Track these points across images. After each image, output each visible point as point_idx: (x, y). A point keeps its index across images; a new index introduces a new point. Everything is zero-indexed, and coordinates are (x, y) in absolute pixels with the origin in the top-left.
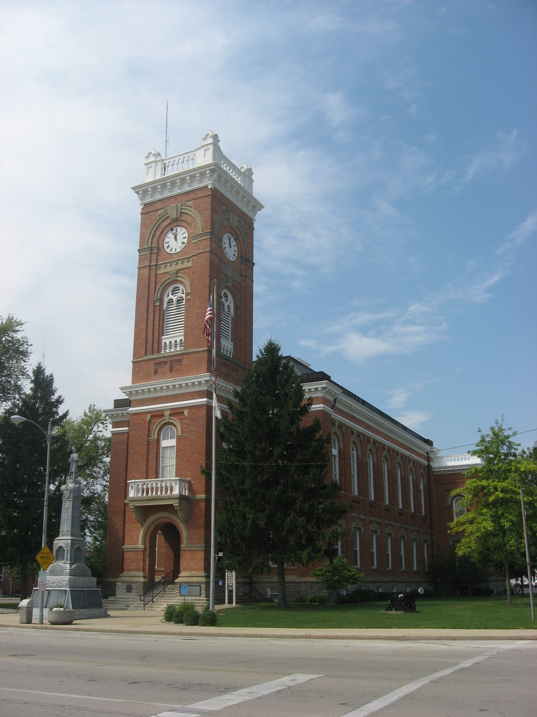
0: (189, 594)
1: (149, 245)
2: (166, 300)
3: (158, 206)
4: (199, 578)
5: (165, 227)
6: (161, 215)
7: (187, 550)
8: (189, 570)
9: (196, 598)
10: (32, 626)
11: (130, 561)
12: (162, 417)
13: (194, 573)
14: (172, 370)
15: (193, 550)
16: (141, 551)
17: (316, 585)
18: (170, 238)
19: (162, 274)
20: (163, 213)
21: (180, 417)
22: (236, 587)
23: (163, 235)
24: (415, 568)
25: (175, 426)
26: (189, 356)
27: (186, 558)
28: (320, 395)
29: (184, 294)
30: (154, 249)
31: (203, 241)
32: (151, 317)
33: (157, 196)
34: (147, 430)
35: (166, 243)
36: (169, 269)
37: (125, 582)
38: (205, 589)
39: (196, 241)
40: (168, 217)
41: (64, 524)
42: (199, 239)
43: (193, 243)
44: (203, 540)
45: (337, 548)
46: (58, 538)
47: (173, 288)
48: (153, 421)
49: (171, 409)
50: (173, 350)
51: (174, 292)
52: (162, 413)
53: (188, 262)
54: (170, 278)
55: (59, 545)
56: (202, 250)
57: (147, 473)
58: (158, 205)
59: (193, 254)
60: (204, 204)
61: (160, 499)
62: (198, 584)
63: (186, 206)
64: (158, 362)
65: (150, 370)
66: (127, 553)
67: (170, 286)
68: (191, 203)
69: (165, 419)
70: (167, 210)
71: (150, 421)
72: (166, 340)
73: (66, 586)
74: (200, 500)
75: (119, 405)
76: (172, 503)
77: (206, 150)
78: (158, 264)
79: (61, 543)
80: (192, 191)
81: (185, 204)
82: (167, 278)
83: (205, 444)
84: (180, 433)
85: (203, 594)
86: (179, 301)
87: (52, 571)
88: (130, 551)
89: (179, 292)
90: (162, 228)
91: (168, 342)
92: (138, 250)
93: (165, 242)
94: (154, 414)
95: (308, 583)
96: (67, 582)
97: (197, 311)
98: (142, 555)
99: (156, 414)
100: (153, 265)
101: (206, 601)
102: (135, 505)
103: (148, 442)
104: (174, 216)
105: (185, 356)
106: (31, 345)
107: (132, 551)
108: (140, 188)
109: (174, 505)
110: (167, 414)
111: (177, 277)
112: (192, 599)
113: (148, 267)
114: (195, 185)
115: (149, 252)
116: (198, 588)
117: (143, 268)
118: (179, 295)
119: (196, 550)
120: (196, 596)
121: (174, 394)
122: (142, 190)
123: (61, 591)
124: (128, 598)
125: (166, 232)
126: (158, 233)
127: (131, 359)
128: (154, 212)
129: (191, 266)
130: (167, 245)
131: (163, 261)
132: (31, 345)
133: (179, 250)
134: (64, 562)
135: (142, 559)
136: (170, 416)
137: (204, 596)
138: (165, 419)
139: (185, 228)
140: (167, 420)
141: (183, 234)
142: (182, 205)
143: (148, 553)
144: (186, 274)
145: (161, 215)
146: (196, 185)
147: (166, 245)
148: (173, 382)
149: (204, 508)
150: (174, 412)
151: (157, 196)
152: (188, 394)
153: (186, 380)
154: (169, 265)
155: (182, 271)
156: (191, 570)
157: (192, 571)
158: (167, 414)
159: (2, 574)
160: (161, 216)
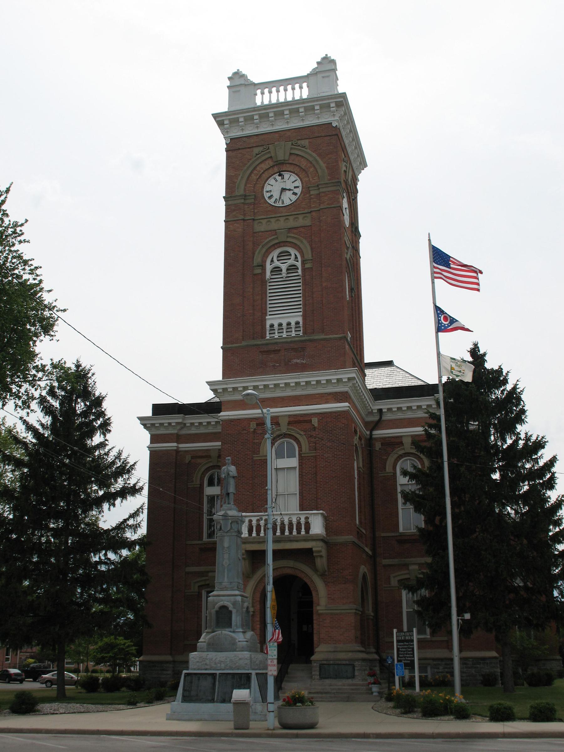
2: (269, 267)
5: (264, 171)
6: (258, 154)
22: (453, 668)
24: (494, 654)
25: (296, 439)
28: (412, 416)
29: (298, 261)
33: (235, 132)
35: (267, 192)
46: (214, 593)
47: (279, 252)
49: (290, 416)
50: (284, 335)
55: (221, 604)
59: (313, 210)
67: (276, 249)
72: (271, 320)
76: (310, 547)
77: (323, 77)
78: (256, 218)
79: (222, 601)
80: (250, 136)
82: (268, 240)
86: (292, 268)
89: (290, 259)
92: (224, 197)
95: (471, 660)
100: (248, 220)
108: (227, 116)
109: (314, 549)
113: (242, 221)
128: (306, 138)
130: (269, 194)
134: (232, 630)
136: (288, 426)
139: (296, 174)
141: (293, 182)
142: (292, 144)
145: (258, 154)
147: (266, 195)
148: (296, 378)
151: (235, 132)
152: (317, 396)
154: (272, 220)
155: (295, 231)
159: (9, 656)
160: (259, 156)
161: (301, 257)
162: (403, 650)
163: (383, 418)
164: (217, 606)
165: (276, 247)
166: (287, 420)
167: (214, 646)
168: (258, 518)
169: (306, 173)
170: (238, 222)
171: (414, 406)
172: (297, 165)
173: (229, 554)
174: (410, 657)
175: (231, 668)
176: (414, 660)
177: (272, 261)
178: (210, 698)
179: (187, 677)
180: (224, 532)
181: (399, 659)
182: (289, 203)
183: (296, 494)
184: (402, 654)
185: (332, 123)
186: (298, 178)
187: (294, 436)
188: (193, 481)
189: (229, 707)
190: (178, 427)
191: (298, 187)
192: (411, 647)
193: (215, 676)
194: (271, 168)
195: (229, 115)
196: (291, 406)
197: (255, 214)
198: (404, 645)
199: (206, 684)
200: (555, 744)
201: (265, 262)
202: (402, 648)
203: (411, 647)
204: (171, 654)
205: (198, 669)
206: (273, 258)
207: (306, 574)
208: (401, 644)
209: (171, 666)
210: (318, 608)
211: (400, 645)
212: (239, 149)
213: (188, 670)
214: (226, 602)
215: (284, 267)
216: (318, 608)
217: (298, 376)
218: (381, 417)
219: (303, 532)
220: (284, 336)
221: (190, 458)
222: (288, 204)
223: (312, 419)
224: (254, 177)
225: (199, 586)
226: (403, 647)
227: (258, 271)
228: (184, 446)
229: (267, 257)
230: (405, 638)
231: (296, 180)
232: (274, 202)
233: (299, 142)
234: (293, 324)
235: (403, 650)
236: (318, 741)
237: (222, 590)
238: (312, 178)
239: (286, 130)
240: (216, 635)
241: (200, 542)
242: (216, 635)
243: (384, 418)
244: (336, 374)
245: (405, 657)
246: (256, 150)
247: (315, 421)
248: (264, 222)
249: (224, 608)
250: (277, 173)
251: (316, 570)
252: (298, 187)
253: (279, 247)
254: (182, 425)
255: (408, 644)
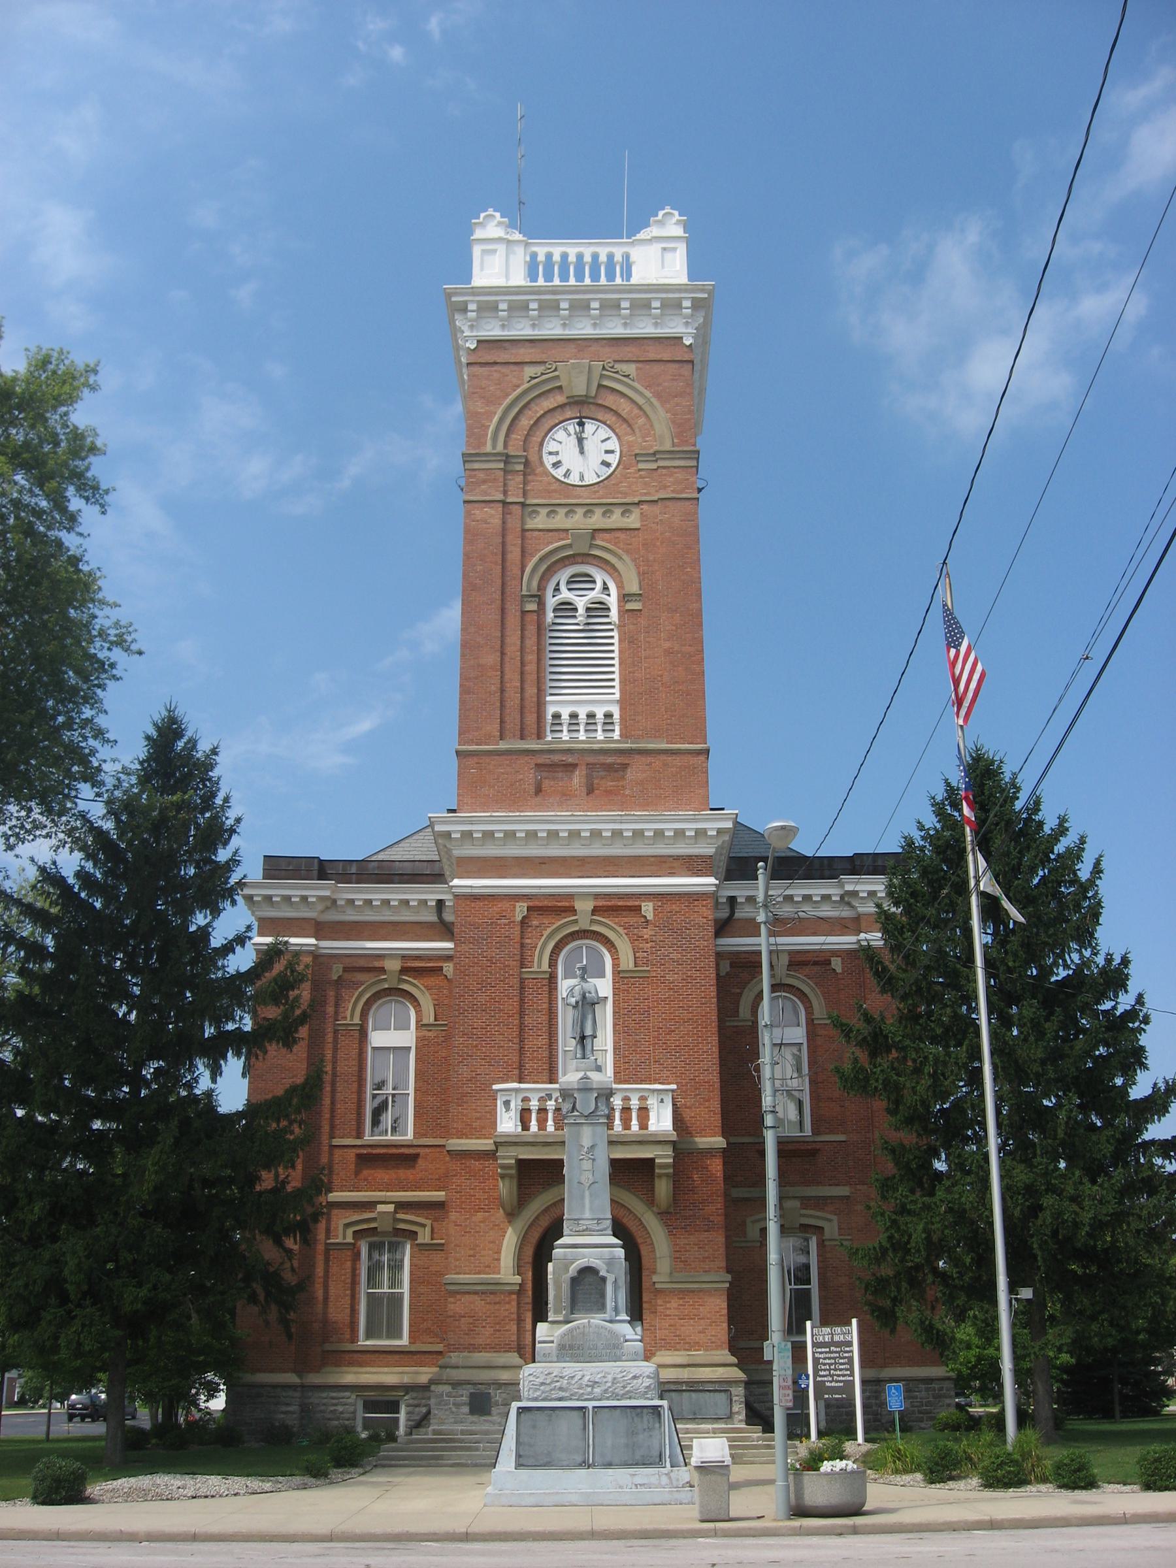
0: (695, 1414)
1: (500, 448)
2: (551, 602)
3: (524, 354)
4: (721, 1370)
5: (546, 413)
7: (672, 1292)
8: (678, 1346)
9: (715, 1426)
10: (794, 1528)
11: (471, 1320)
12: (563, 914)
13: (699, 1355)
14: (593, 791)
15: (693, 1291)
16: (511, 1293)
17: (923, 1386)
18: (561, 443)
19: (540, 530)
20: (543, 374)
21: (626, 920)
23: (541, 427)
26: (649, 759)
27: (668, 1312)
29: (609, 595)
30: (513, 461)
31: (676, 470)
32: (513, 639)
34: (517, 946)
35: (550, 453)
36: (560, 520)
37: (468, 1383)
38: (743, 1400)
39: (654, 466)
40: (560, 387)
41: (582, 1197)
42: (661, 463)
43: (640, 470)
44: (723, 1264)
45: (402, 1293)
48: (535, 923)
49: (597, 896)
51: (581, 581)
52: (567, 904)
53: (567, 514)
54: (570, 546)
56: (673, 491)
57: (521, 1067)
58: (522, 351)
59: (644, 499)
60: (673, 380)
61: (640, 1143)
62: (723, 1387)
63: (617, 372)
64: (548, 762)
65: (521, 780)
66: (458, 1297)
67: (565, 566)
68: (631, 369)
69: (576, 921)
70: (555, 370)
71: (524, 922)
73: (646, 1393)
74: (710, 1152)
75: (283, 872)
77: (664, 249)
78: (528, 502)
81: (612, 367)
82: (551, 547)
83: (715, 1000)
84: (627, 962)
85: (738, 1413)
87: (571, 1347)
88: (469, 1293)
89: (593, 589)
90: (537, 412)
91: (565, 713)
93: (545, 450)
94: (537, 903)
96: (647, 1382)
97: (667, 645)
98: (514, 1303)
99: (546, 903)
101: (760, 1434)
102: (521, 1157)
103: (522, 981)
104: (580, 389)
105: (637, 756)
106: (140, 653)
107: (476, 1293)
109: (657, 1161)
110: (584, 907)
111: (591, 546)
112: (713, 1428)
114: (611, 329)
115: (501, 465)
116: (723, 1396)
117: (483, 505)
118: (592, 595)
119: (701, 1290)
120: (717, 1419)
121: (608, 854)
122: (478, 301)
123: (639, 1410)
124: (487, 1433)
125: (547, 427)
126: (525, 422)
127: (453, 743)
128: (513, 367)
129: (637, 525)
130: (553, 459)
131: (542, 498)
132: (140, 653)
133: (591, 479)
134: (607, 1316)
135: (515, 1316)
136: (592, 915)
137: (741, 1421)
138: (576, 921)
139: (609, 426)
140: (584, 924)
141: (603, 441)
142: (604, 368)
143: (529, 1300)
144: (621, 545)
146: (645, 328)
147: (549, 461)
148: (614, 822)
149: (720, 1174)
150: (609, 904)
151: (519, 328)
152: (652, 859)
153: (660, 821)
155: (607, 536)
156: (687, 1346)
157: (690, 1350)
158: (584, 907)
161: (618, 587)
162: (827, 1361)
163: (736, 914)
164: (573, 1270)
165: (567, 563)
166: (589, 905)
167: (570, 1350)
168: (543, 1095)
169: (630, 426)
170: (492, 505)
171: (798, 895)
172: (612, 410)
173: (594, 1160)
174: (844, 1376)
175: (616, 1397)
176: (853, 1382)
177: (557, 589)
178: (579, 1459)
179: (522, 1415)
180: (582, 1115)
181: (819, 1379)
182: (595, 481)
183: (606, 1051)
184: (825, 1370)
185: (682, 338)
186: (612, 435)
187: (604, 936)
188: (345, 1018)
189: (684, 1474)
190: (320, 907)
191: (612, 452)
192: (846, 1355)
193: (584, 1413)
194: (559, 409)
195: (478, 295)
196: (600, 877)
197: (525, 494)
198: (830, 1352)
199: (567, 1426)
200: (810, 1546)
201: (545, 589)
202: (825, 1359)
203: (846, 1355)
204: (294, 1371)
205: (543, 1400)
206: (558, 584)
207: (629, 1209)
208: (823, 1350)
209: (297, 1394)
210: (655, 1278)
211: (821, 1353)
212: (496, 363)
213: (520, 1400)
214: (589, 1258)
215: (581, 603)
216: (655, 1278)
217: (619, 818)
218: (732, 913)
219: (635, 1125)
220: (581, 738)
221: (341, 970)
222: (591, 482)
223: (643, 904)
224: (525, 422)
225: (355, 1232)
226: (828, 1355)
227: (532, 606)
228: (331, 946)
229: (548, 580)
230: (832, 1338)
231: (608, 439)
232: (565, 475)
233: (618, 366)
234: (600, 716)
235: (827, 1361)
236: (378, 1549)
237: (580, 1233)
238: (643, 438)
239: (591, 339)
240: (579, 1328)
241: (358, 1142)
242: (579, 1328)
243: (737, 915)
244: (695, 820)
245: (832, 1376)
246: (530, 371)
247: (648, 909)
248: (544, 511)
249: (588, 1271)
250: (576, 418)
251: (651, 1201)
252: (612, 452)
253: (573, 564)
254: (329, 904)
255: (838, 1349)
